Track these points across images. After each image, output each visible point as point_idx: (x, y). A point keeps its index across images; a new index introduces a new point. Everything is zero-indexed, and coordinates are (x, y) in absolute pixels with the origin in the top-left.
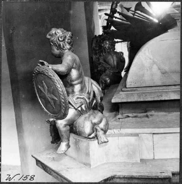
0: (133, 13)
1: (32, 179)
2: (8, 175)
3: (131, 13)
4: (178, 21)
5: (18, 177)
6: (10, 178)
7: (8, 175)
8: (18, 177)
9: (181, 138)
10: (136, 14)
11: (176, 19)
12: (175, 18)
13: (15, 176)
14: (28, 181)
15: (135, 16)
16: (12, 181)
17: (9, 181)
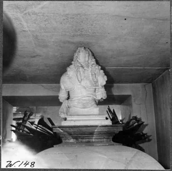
0: (36, 126)
1: (32, 166)
2: (7, 162)
3: (34, 127)
4: (63, 138)
5: (19, 163)
6: (11, 164)
7: (7, 162)
8: (19, 163)
9: (96, 170)
10: (38, 128)
11: (62, 137)
12: (61, 136)
13: (15, 163)
14: (28, 167)
15: (38, 130)
16: (13, 167)
17: (10, 167)
